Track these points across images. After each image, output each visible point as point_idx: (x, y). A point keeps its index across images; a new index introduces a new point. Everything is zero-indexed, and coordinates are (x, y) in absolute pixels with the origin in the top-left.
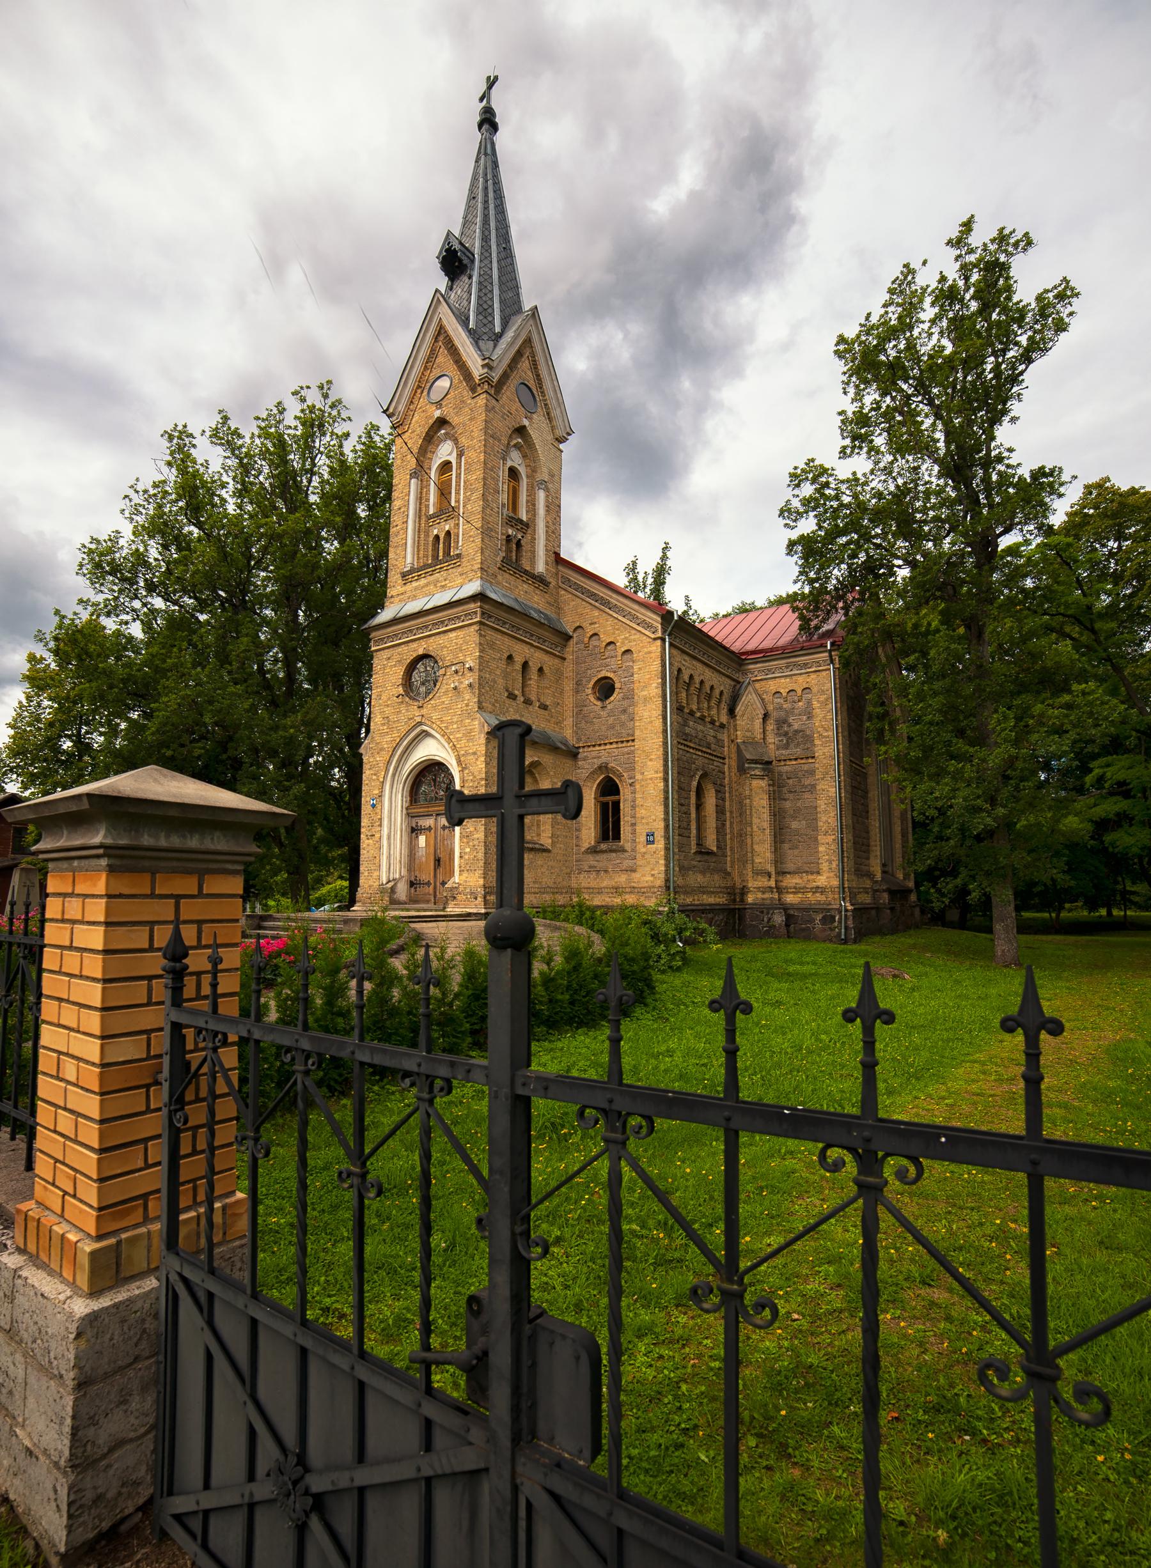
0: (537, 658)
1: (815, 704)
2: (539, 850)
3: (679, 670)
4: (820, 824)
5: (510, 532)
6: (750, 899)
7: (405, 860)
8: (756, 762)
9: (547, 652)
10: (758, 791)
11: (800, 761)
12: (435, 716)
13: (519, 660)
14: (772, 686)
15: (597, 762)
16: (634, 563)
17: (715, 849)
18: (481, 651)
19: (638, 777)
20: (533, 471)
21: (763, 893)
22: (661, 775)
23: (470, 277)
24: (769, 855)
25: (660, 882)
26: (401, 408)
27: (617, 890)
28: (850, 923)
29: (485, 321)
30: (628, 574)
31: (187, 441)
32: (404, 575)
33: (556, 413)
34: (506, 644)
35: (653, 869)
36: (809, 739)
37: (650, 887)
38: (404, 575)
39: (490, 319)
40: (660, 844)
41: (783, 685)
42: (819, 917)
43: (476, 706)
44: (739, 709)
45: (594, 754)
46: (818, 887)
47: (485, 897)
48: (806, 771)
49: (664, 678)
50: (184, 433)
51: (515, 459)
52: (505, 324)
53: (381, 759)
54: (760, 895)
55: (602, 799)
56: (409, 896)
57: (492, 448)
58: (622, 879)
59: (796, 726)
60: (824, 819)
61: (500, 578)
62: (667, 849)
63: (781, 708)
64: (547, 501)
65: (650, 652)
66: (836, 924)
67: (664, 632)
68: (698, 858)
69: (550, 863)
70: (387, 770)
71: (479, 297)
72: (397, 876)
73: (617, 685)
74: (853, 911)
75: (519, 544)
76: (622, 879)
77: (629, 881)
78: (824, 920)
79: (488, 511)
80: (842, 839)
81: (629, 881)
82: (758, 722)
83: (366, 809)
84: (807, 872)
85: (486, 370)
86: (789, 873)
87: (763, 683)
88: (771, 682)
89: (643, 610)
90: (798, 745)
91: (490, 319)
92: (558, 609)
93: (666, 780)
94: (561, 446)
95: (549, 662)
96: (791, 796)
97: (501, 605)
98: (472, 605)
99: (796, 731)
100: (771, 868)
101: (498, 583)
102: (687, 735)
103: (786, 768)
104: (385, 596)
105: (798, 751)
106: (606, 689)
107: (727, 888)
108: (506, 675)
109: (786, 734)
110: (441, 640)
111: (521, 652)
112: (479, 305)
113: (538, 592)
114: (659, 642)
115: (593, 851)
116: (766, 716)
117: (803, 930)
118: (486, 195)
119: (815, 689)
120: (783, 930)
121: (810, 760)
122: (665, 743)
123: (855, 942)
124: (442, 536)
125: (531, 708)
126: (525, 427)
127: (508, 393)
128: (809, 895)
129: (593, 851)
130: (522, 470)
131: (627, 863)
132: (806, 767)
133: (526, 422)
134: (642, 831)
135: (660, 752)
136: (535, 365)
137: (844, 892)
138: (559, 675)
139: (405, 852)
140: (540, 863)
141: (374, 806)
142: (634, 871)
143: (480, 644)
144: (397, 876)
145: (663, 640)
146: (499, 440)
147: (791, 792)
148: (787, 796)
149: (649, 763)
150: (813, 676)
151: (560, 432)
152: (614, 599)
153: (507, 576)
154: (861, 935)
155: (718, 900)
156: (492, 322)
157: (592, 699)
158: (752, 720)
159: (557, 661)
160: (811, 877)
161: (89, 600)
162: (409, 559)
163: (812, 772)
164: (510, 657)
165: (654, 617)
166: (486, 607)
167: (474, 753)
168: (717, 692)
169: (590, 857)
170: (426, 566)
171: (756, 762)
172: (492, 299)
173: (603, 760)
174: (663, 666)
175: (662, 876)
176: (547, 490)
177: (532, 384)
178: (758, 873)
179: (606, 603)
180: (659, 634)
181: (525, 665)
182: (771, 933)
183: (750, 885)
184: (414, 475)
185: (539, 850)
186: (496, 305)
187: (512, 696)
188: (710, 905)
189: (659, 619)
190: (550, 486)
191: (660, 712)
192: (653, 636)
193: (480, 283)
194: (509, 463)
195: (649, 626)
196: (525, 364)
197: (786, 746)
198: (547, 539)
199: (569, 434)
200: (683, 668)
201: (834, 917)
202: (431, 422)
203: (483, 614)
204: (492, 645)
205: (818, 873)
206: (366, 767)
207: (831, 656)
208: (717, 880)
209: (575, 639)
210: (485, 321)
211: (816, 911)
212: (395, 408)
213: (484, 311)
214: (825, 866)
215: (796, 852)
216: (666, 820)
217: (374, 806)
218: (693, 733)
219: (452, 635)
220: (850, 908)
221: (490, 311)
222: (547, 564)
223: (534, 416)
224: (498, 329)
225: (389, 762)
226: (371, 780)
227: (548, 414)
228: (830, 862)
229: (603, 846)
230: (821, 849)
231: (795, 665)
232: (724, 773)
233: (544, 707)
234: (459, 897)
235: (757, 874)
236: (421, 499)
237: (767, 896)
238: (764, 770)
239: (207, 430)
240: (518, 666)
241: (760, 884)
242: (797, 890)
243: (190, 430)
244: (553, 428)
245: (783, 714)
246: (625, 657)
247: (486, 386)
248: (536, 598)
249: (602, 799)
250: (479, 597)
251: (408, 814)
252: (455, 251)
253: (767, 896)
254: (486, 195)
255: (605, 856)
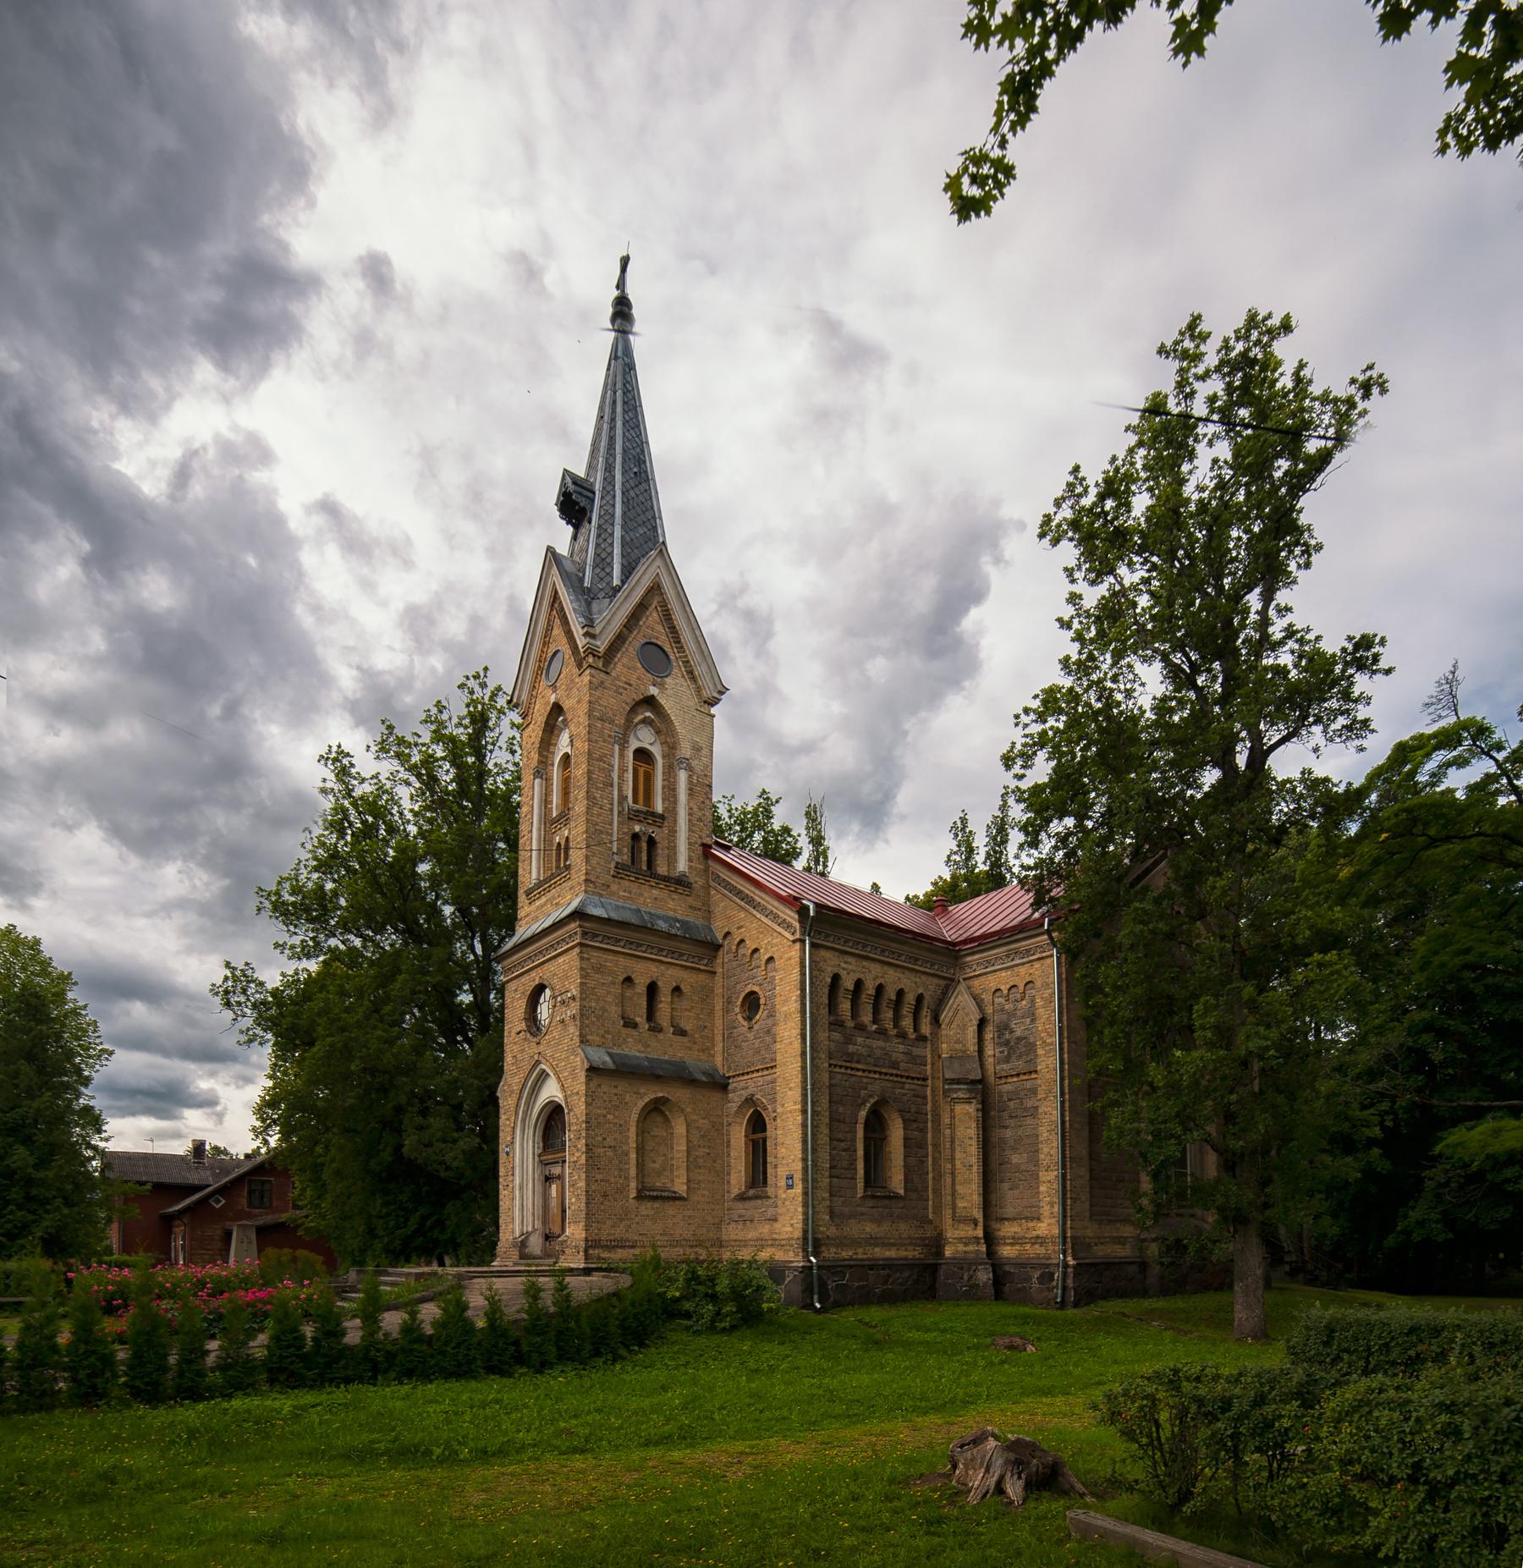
0: (668, 977)
1: (1039, 1002)
2: (668, 1198)
3: (836, 978)
4: (1042, 1156)
5: (637, 828)
6: (948, 1252)
7: (539, 1212)
8: (958, 1081)
9: (686, 968)
10: (964, 1120)
11: (1022, 1077)
12: (549, 1053)
13: (641, 983)
14: (992, 982)
15: (745, 1094)
16: (964, 821)
17: (902, 1192)
18: (582, 977)
19: (779, 1110)
20: (671, 748)
21: (966, 1244)
22: (799, 1107)
23: (590, 522)
24: (977, 1198)
25: (798, 1234)
26: (524, 697)
27: (761, 1243)
28: (1070, 1282)
29: (602, 574)
30: (956, 835)
31: (345, 761)
32: (528, 893)
33: (700, 670)
34: (621, 966)
35: (792, 1218)
36: (1031, 1048)
37: (789, 1239)
38: (528, 893)
39: (608, 570)
40: (798, 1189)
41: (1002, 979)
42: (1037, 1274)
43: (578, 1040)
44: (945, 1016)
45: (742, 1084)
46: (1038, 1237)
47: (586, 1251)
48: (1029, 1090)
49: (803, 990)
50: (342, 753)
51: (644, 738)
52: (627, 571)
53: (512, 1102)
54: (961, 1248)
55: (752, 1137)
56: (544, 1250)
57: (601, 732)
58: (765, 1229)
59: (1018, 1033)
60: (1046, 1150)
61: (614, 887)
62: (805, 1194)
63: (1003, 1010)
64: (690, 782)
65: (790, 959)
66: (1054, 1283)
67: (803, 934)
68: (870, 1203)
69: (687, 1213)
70: (517, 1113)
71: (598, 545)
72: (530, 1229)
73: (762, 1001)
74: (1074, 1267)
75: (652, 842)
76: (765, 1229)
77: (772, 1232)
78: (1041, 1279)
79: (595, 810)
80: (1064, 1176)
81: (772, 1232)
82: (972, 1031)
83: (502, 1158)
84: (1026, 1218)
85: (588, 639)
86: (1008, 1219)
87: (982, 979)
88: (991, 977)
89: (776, 904)
90: (1020, 1057)
91: (608, 570)
92: (708, 914)
93: (804, 1112)
94: (713, 711)
95: (688, 980)
96: (1012, 1122)
97: (608, 921)
98: (573, 925)
99: (1019, 1039)
100: (978, 1214)
101: (613, 894)
102: (848, 1054)
103: (1007, 1087)
104: (516, 919)
105: (1020, 1065)
106: (752, 1003)
107: (922, 1239)
108: (622, 1001)
109: (1007, 1043)
110: (550, 967)
111: (644, 973)
112: (597, 555)
113: (675, 896)
114: (798, 945)
115: (742, 1198)
116: (982, 1023)
117: (1019, 1290)
118: (614, 411)
119: (1038, 984)
120: (991, 1291)
121: (1033, 1076)
122: (804, 1068)
123: (1076, 1305)
124: (563, 843)
125: (661, 1036)
126: (653, 696)
127: (625, 660)
128: (1028, 1247)
129: (742, 1198)
130: (656, 751)
131: (771, 1212)
132: (1028, 1085)
133: (653, 691)
134: (782, 1172)
135: (798, 1080)
136: (667, 616)
137: (1064, 1243)
138: (707, 994)
139: (539, 1202)
140: (671, 1212)
141: (507, 1154)
142: (775, 1220)
143: (582, 969)
144: (530, 1229)
145: (802, 941)
146: (612, 722)
147: (1011, 1117)
148: (1007, 1123)
149: (789, 1093)
150: (1037, 965)
151: (709, 692)
152: (759, 897)
153: (627, 883)
154: (1085, 1297)
155: (910, 1254)
156: (610, 575)
157: (741, 1019)
158: (964, 1028)
159: (702, 977)
160: (1031, 1224)
161: (285, 943)
162: (534, 875)
163: (1034, 1091)
164: (628, 980)
165: (792, 914)
166: (586, 924)
167: (577, 1093)
168: (910, 998)
169: (740, 1205)
170: (552, 876)
171: (958, 1081)
172: (612, 545)
173: (750, 1091)
174: (803, 974)
175: (800, 1225)
176: (690, 769)
177: (663, 640)
178: (958, 1220)
179: (750, 901)
180: (798, 936)
181: (652, 989)
182: (972, 1294)
183: (949, 1235)
184: (538, 773)
185: (668, 1198)
186: (617, 551)
187: (630, 1024)
188: (887, 1259)
189: (796, 917)
190: (694, 763)
191: (798, 1031)
192: (792, 938)
193: (600, 526)
194: (634, 744)
195: (789, 926)
196: (652, 617)
197: (1007, 1060)
198: (690, 830)
199: (722, 693)
200: (843, 974)
201: (1053, 1274)
202: (549, 708)
203: (584, 934)
204: (599, 969)
205: (1039, 1219)
206: (502, 1111)
207: (1051, 938)
208: (904, 1229)
209: (726, 948)
210: (602, 574)
211: (1034, 1267)
212: (519, 697)
213: (602, 562)
214: (1045, 1210)
215: (1016, 1192)
216: (804, 1160)
217: (507, 1154)
218: (863, 1051)
219: (561, 960)
220: (1071, 1262)
221: (608, 560)
222: (690, 860)
223: (668, 680)
224: (616, 582)
225: (518, 1106)
226: (505, 1125)
227: (691, 672)
228: (1051, 1204)
229: (751, 1192)
230: (1043, 1188)
231: (1017, 952)
232: (925, 1097)
233: (682, 1033)
234: (568, 1251)
235: (959, 1222)
236: (546, 801)
237: (971, 1248)
238: (969, 1091)
239: (372, 744)
240: (641, 989)
241: (963, 1234)
242: (1016, 1240)
243: (346, 749)
244: (699, 690)
245: (1004, 1017)
246: (770, 966)
247: (591, 659)
248: (671, 904)
249: (752, 1137)
250: (578, 915)
251: (541, 1161)
252: (570, 494)
253: (971, 1248)
254: (614, 411)
255: (753, 1203)
